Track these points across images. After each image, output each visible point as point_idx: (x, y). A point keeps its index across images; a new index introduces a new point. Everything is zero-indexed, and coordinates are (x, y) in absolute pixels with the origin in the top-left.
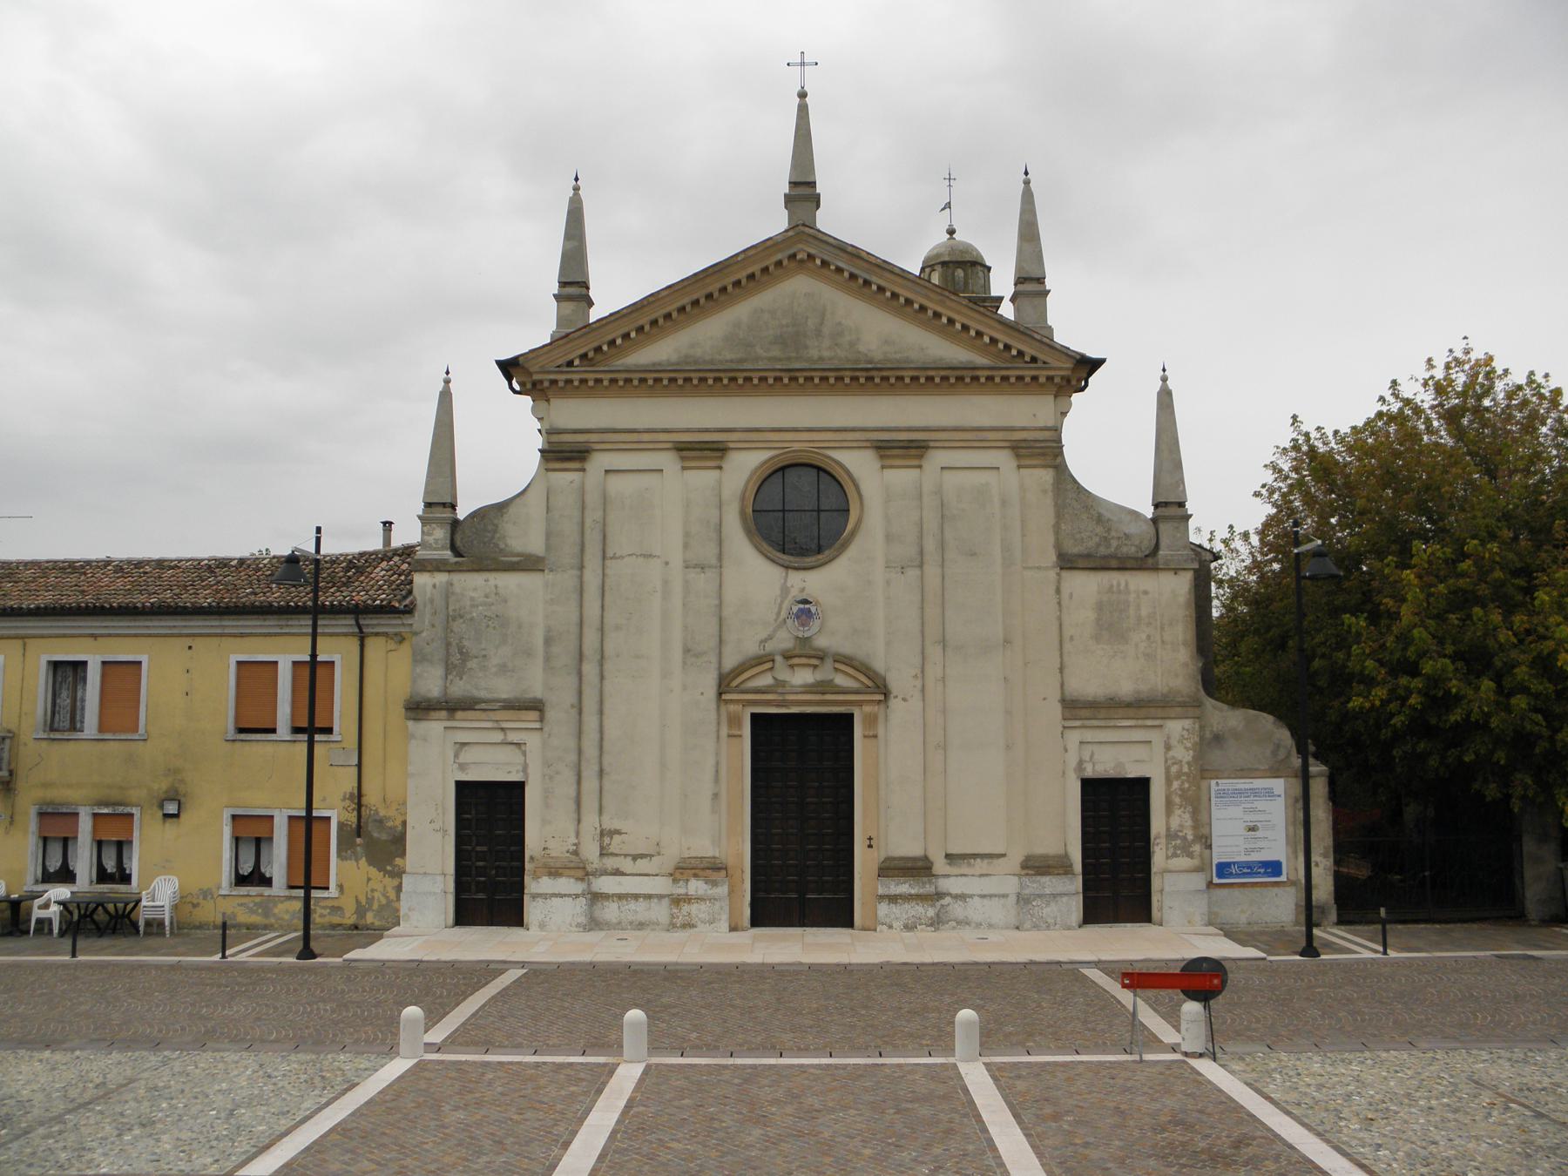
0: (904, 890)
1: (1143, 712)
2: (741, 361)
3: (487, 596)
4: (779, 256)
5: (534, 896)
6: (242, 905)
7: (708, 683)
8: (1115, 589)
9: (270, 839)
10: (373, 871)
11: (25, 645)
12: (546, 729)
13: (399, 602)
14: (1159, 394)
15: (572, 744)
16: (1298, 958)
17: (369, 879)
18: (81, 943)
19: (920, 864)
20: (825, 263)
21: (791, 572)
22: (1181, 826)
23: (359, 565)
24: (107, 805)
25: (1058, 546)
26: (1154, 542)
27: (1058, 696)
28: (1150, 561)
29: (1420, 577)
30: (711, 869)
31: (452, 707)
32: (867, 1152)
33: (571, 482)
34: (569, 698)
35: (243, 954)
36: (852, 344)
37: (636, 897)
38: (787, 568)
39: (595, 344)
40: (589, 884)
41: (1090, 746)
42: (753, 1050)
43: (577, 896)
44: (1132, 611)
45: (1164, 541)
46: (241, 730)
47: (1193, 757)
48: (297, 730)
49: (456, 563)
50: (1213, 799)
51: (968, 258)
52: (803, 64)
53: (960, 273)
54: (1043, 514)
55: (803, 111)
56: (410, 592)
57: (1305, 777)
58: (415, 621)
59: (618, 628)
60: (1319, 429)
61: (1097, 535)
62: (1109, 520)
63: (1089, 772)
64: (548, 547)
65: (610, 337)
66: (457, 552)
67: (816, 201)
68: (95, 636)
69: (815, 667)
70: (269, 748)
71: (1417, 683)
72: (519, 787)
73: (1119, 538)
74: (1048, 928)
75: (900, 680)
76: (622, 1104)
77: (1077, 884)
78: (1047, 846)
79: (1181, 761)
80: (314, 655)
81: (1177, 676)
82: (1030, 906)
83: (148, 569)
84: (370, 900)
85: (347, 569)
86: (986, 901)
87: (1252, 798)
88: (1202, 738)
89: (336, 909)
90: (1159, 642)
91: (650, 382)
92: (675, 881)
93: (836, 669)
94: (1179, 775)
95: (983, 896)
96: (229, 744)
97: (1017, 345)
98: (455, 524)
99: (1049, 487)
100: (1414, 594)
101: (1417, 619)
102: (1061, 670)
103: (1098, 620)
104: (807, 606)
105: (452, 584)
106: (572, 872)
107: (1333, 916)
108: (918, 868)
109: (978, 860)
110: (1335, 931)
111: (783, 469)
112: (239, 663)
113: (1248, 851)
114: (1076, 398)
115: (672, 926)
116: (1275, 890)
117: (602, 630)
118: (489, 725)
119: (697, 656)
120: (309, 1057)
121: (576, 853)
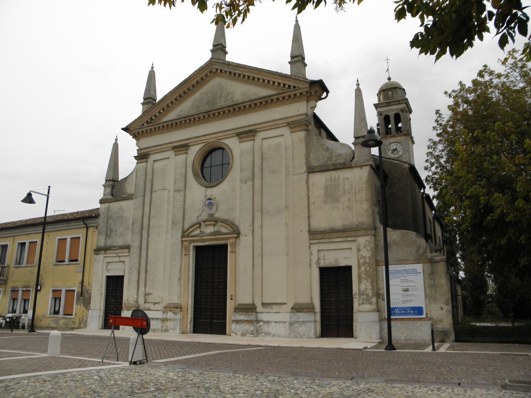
0: (242, 318)
1: (346, 234)
6: (51, 320)
8: (333, 179)
10: (84, 308)
11: (14, 238)
12: (130, 256)
14: (356, 90)
15: (137, 261)
17: (83, 312)
19: (250, 307)
21: (208, 189)
22: (366, 289)
25: (308, 162)
27: (306, 229)
33: (143, 166)
34: (136, 244)
36: (231, 98)
38: (207, 187)
39: (150, 117)
41: (323, 252)
44: (341, 188)
47: (371, 255)
51: (393, 86)
53: (390, 93)
59: (154, 217)
61: (326, 156)
62: (332, 149)
63: (322, 264)
65: (154, 114)
68: (28, 234)
72: (122, 277)
73: (336, 156)
75: (244, 228)
77: (318, 317)
78: (304, 299)
79: (365, 257)
81: (363, 216)
82: (293, 327)
84: (82, 319)
86: (277, 324)
87: (405, 274)
90: (354, 201)
93: (222, 226)
94: (364, 263)
95: (276, 322)
96: (54, 266)
99: (303, 139)
102: (309, 218)
103: (325, 194)
104: (211, 201)
105: (110, 207)
107: (453, 337)
108: (250, 309)
109: (275, 306)
112: (59, 240)
113: (404, 302)
116: (420, 322)
118: (115, 255)
119: (176, 224)
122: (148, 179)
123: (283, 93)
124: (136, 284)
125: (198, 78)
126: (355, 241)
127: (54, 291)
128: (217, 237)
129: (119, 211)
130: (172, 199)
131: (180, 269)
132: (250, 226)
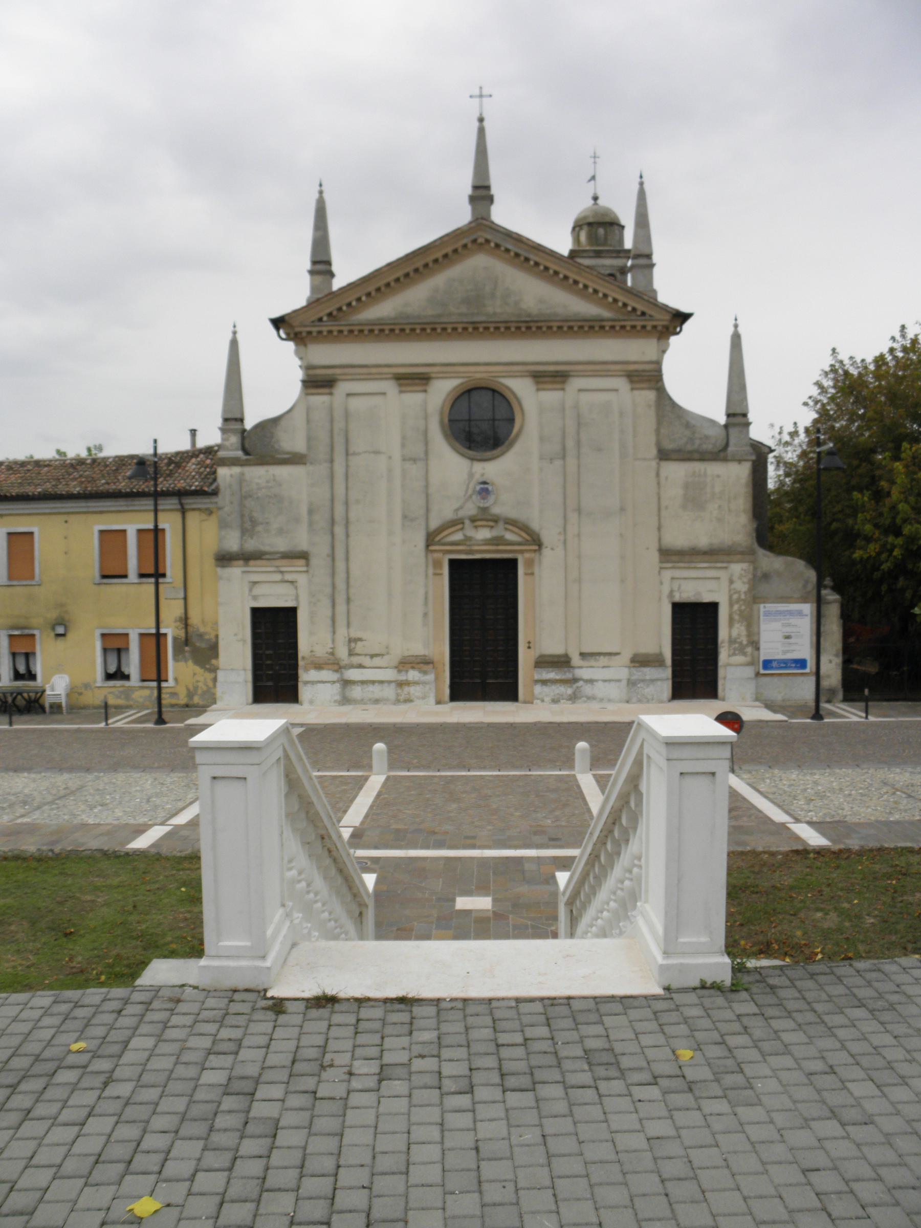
2: (439, 316)
3: (268, 482)
4: (465, 241)
5: (306, 683)
7: (420, 539)
9: (127, 649)
10: (198, 669)
13: (208, 487)
16: (809, 721)
17: (195, 674)
18: (14, 718)
19: (562, 659)
20: (497, 246)
23: (178, 460)
24: (17, 628)
25: (658, 444)
26: (725, 441)
28: (722, 455)
29: (906, 466)
30: (423, 663)
31: (247, 557)
32: (518, 814)
34: (325, 550)
35: (119, 722)
37: (373, 682)
39: (337, 306)
40: (342, 674)
42: (451, 768)
43: (334, 682)
45: (732, 441)
46: (104, 577)
48: (142, 576)
49: (247, 460)
50: (762, 617)
51: (607, 219)
52: (481, 96)
53: (601, 231)
54: (649, 421)
55: (481, 132)
56: (215, 480)
57: (820, 602)
58: (219, 500)
60: (851, 358)
62: (694, 426)
63: (677, 598)
64: (309, 447)
65: (347, 301)
66: (246, 452)
67: (490, 199)
69: (492, 527)
70: (123, 589)
71: (900, 541)
73: (701, 439)
74: (648, 702)
75: (549, 536)
76: (375, 793)
77: (668, 672)
78: (648, 647)
80: (156, 526)
83: (29, 467)
84: (196, 688)
85: (169, 464)
86: (607, 684)
88: (754, 576)
89: (174, 694)
91: (376, 332)
92: (399, 671)
93: (506, 529)
95: (605, 681)
97: (632, 303)
98: (244, 431)
100: (901, 479)
101: (902, 496)
102: (659, 528)
104: (486, 486)
106: (330, 667)
107: (840, 695)
108: (561, 662)
109: (602, 657)
110: (842, 706)
111: (469, 391)
112: (102, 532)
113: (785, 652)
114: (673, 339)
115: (397, 701)
116: (802, 678)
117: (347, 504)
119: (412, 520)
120: (182, 775)
121: (332, 654)
122: (336, 430)
123: (624, 320)
124: (329, 622)
125: (449, 250)
126: (726, 568)
127: (104, 636)
128: (501, 548)
129: (270, 485)
130: (397, 472)
131: (426, 598)
132: (560, 533)
